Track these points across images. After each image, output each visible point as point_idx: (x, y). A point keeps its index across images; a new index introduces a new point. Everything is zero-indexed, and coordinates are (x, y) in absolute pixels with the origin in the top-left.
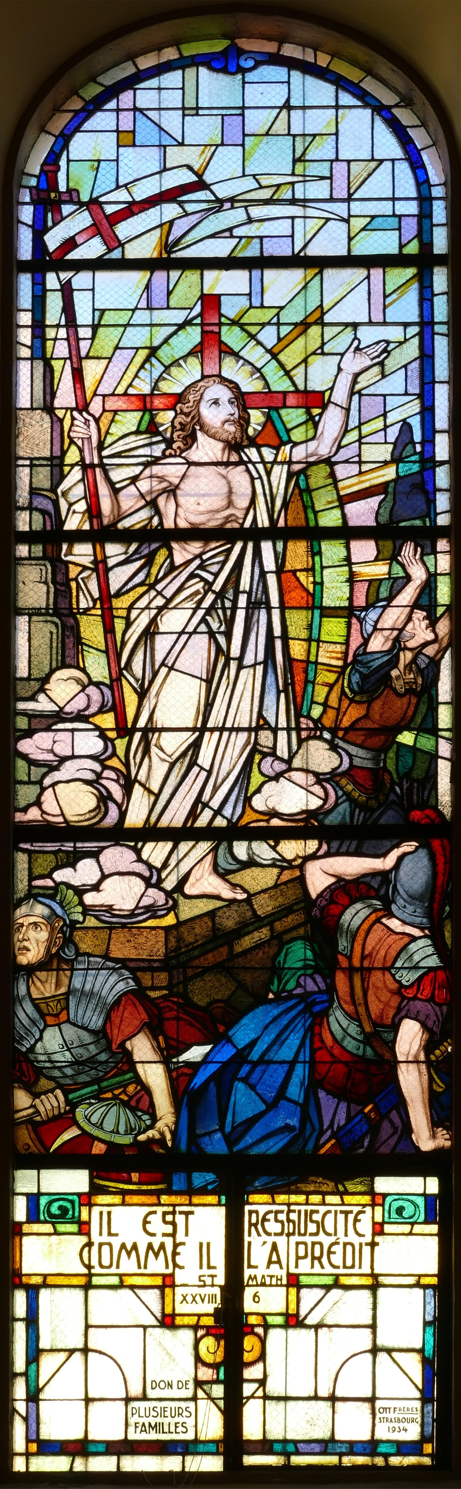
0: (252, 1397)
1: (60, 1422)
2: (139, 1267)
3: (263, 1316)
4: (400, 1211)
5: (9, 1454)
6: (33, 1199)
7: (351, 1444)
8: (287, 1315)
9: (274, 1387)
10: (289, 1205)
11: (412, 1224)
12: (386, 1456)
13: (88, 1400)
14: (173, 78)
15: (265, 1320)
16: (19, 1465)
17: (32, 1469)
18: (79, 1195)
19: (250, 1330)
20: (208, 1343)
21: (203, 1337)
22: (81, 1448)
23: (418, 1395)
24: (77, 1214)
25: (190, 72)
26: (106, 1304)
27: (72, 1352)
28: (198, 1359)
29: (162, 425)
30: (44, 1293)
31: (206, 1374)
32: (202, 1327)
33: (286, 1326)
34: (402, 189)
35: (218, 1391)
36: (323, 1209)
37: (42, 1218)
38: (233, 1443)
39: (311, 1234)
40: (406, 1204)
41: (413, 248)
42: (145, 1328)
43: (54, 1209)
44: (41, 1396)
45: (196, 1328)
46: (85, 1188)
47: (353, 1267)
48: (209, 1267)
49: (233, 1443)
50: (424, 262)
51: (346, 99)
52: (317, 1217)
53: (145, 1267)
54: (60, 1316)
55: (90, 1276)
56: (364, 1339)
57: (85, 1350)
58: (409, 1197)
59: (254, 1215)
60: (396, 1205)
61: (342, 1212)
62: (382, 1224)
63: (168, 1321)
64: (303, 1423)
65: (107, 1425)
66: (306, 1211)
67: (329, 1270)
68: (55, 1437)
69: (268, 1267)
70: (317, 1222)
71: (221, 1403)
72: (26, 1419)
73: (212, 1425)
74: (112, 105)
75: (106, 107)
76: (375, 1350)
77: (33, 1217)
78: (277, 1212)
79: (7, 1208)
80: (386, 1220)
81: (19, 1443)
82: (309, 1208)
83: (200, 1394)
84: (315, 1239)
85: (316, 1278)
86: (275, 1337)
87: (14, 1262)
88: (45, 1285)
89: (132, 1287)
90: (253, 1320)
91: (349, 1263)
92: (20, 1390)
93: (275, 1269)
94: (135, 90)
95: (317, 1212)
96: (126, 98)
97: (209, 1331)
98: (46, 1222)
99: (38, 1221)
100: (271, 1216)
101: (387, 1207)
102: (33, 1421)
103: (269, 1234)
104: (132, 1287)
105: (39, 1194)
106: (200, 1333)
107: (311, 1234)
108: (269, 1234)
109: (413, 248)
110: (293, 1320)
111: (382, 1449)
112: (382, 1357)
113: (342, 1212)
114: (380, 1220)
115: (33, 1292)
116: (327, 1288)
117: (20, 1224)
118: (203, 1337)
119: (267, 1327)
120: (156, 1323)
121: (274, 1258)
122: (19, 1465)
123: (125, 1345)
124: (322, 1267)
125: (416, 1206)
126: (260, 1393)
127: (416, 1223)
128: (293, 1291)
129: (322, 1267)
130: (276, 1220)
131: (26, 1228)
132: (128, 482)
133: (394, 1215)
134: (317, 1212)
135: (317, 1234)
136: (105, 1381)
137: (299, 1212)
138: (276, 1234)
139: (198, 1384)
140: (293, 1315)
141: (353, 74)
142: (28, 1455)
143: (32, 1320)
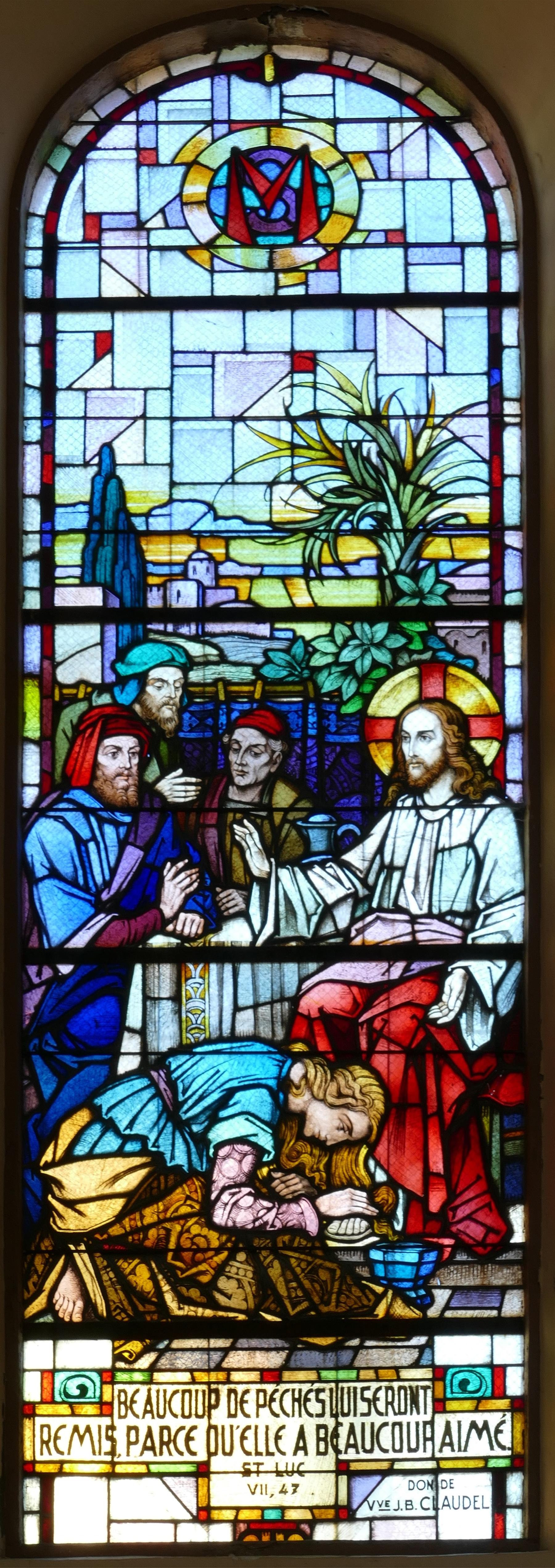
4: (464, 1384)
8: (336, 1507)
14: (201, 88)
18: (100, 1372)
24: (98, 1394)
25: (221, 81)
29: (122, 691)
30: (58, 1482)
36: (374, 1385)
39: (363, 1415)
46: (106, 1363)
47: (401, 1450)
51: (408, 113)
52: (368, 1394)
53: (465, 1450)
55: (113, 1464)
58: (87, 1374)
59: (46, 1430)
60: (460, 1376)
62: (445, 1399)
66: (349, 1388)
69: (142, 1454)
74: (131, 117)
75: (125, 119)
78: (319, 1391)
80: (449, 1395)
82: (359, 1385)
87: (519, 1427)
88: (61, 1473)
89: (161, 1475)
91: (397, 1447)
94: (157, 102)
96: (147, 111)
98: (63, 1402)
99: (53, 1402)
100: (312, 1396)
101: (448, 1382)
103: (311, 1415)
104: (161, 1475)
105: (53, 1372)
107: (363, 1415)
108: (311, 1415)
114: (441, 1396)
115: (47, 1482)
117: (33, 1405)
120: (189, 1517)
124: (170, 1454)
125: (481, 1378)
128: (343, 1479)
129: (170, 1454)
130: (318, 1400)
131: (42, 1409)
132: (285, 125)
133: (456, 1389)
134: (368, 1388)
135: (368, 1414)
138: (318, 1416)
140: (343, 1507)
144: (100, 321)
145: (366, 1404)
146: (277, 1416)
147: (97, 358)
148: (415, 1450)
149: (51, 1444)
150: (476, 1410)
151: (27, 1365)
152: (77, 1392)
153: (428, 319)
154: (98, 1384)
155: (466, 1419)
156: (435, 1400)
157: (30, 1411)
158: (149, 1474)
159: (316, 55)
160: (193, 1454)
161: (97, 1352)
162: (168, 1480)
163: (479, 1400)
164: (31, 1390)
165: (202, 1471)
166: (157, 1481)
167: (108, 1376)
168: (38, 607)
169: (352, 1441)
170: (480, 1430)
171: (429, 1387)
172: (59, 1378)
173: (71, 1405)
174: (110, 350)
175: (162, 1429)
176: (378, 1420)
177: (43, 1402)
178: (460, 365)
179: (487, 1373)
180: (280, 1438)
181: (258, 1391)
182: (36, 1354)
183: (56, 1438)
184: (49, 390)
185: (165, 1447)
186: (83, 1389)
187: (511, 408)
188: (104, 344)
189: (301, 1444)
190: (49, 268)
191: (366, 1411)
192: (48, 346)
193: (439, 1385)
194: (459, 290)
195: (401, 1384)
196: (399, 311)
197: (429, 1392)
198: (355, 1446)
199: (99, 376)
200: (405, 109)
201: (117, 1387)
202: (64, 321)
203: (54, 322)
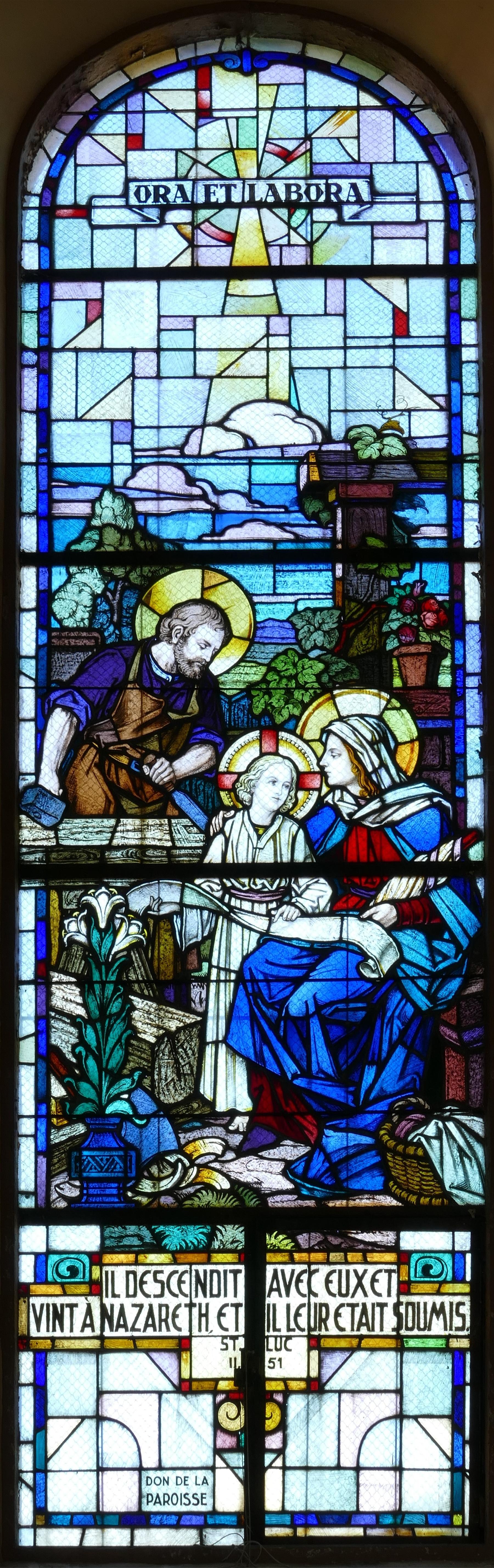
0: (270, 1466)
1: (68, 1493)
2: (446, 1329)
3: (285, 1380)
4: (426, 1269)
5: (12, 1526)
6: (41, 1259)
7: (378, 1514)
8: (308, 1380)
9: (293, 1456)
10: (309, 1264)
11: (441, 1283)
12: (412, 1527)
13: (100, 1469)
15: (286, 1385)
16: (26, 1538)
17: (41, 1543)
18: (90, 1255)
19: (269, 1396)
20: (230, 1409)
21: (222, 1402)
22: (99, 1519)
23: (447, 1465)
26: (125, 1369)
27: (83, 1418)
28: (217, 1426)
30: (52, 1357)
31: (225, 1441)
32: (222, 1392)
33: (304, 1392)
34: (168, 159)
35: (237, 1460)
37: (50, 1279)
38: (253, 1514)
40: (431, 1262)
41: (437, 259)
42: (160, 1393)
43: (63, 1269)
44: (51, 1465)
45: (215, 1392)
48: (275, 1329)
49: (253, 1514)
50: (450, 271)
51: (367, 100)
52: (162, 1277)
54: (70, 1382)
56: (388, 1405)
57: (99, 1418)
58: (437, 1255)
59: (164, 1309)
61: (231, 1271)
63: (186, 1387)
64: (330, 1494)
65: (120, 1496)
67: (174, 1333)
68: (447, 1497)
69: (82, 1330)
70: (162, 1282)
71: (241, 1473)
72: (33, 1489)
73: (230, 1496)
76: (400, 1416)
77: (41, 1278)
79: (13, 1268)
81: (26, 1514)
83: (219, 1463)
84: (162, 1301)
85: (77, 1342)
86: (296, 1404)
88: (54, 1349)
89: (147, 1351)
90: (270, 1386)
92: (26, 1458)
93: (88, 1332)
95: (162, 1272)
97: (230, 1397)
98: (55, 1283)
99: (46, 1282)
100: (149, 1278)
102: (39, 1490)
103: (148, 1296)
106: (220, 1398)
108: (148, 1296)
109: (437, 259)
110: (315, 1386)
111: (408, 1520)
112: (409, 1424)
113: (231, 1271)
116: (352, 1350)
117: (26, 1286)
118: (222, 1402)
119: (287, 1393)
120: (170, 1388)
121: (150, 1322)
122: (26, 1538)
123: (137, 1412)
126: (279, 1463)
127: (445, 1282)
128: (315, 1354)
130: (156, 1280)
134: (162, 1272)
136: (118, 1448)
137: (340, 1272)
139: (218, 1452)
141: (370, 73)
142: (35, 1526)
143: (40, 1387)
144: (92, 289)
145: (159, 1285)
146: (176, 1296)
147: (88, 324)
148: (412, 1329)
149: (170, 1320)
150: (438, 1293)
151: (24, 1247)
152: (68, 1274)
153: (395, 288)
154: (87, 1265)
155: (430, 1300)
156: (400, 1283)
157: (25, 1291)
158: (136, 1349)
159: (293, 48)
160: (179, 1329)
161: (86, 1237)
162: (154, 1355)
163: (441, 1283)
164: (26, 1272)
165: (183, 1346)
166: (143, 1356)
167: (96, 1258)
168: (34, 550)
169: (364, 1321)
170: (438, 1311)
171: (394, 1271)
172: (53, 1259)
173: (62, 1285)
174: (101, 315)
175: (160, 1306)
176: (172, 1302)
177: (35, 1283)
178: (362, 329)
179: (447, 1258)
180: (177, 1316)
181: (128, 1273)
182: (32, 1238)
183: (175, 1316)
184: (46, 351)
185: (163, 1324)
186: (73, 1271)
187: (30, 358)
188: (95, 311)
189: (88, 1322)
190: (46, 241)
191: (159, 1292)
192: (45, 313)
193: (404, 1268)
194: (423, 262)
195: (214, 1267)
196: (369, 281)
197: (394, 1276)
198: (367, 1324)
199: (90, 338)
200: (363, 95)
201: (105, 1269)
202: (61, 289)
203: (52, 291)
